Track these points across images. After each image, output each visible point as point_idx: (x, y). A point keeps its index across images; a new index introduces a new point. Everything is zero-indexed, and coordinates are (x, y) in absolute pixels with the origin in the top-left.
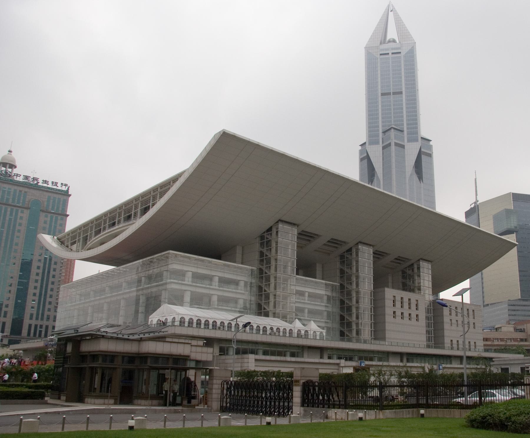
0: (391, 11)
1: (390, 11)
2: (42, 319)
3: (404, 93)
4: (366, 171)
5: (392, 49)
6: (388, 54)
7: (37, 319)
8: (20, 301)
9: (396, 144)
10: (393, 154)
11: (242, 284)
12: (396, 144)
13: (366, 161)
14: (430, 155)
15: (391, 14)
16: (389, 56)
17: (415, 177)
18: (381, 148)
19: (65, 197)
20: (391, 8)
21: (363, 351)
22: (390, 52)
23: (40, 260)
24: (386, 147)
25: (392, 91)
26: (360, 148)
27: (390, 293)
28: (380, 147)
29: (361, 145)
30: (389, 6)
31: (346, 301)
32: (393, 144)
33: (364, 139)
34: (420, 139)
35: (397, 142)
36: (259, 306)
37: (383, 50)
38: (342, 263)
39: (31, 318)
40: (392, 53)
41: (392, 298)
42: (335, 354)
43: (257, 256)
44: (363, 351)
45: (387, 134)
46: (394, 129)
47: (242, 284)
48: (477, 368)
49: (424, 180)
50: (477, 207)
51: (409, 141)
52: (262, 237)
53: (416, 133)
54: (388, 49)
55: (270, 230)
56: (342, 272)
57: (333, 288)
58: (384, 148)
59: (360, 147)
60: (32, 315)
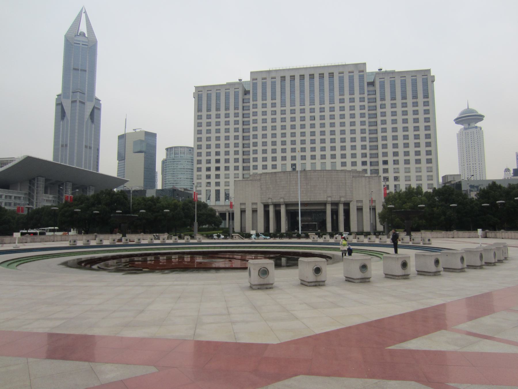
0: (84, 13)
1: (83, 12)
3: (87, 71)
5: (83, 41)
6: (79, 44)
10: (78, 108)
11: (22, 198)
13: (60, 107)
15: (83, 15)
16: (79, 46)
17: (90, 121)
20: (83, 11)
21: (418, 172)
22: (81, 43)
24: (73, 102)
26: (57, 97)
28: (70, 101)
29: (58, 95)
30: (82, 9)
31: (31, 199)
32: (78, 101)
33: (59, 91)
34: (94, 100)
35: (81, 100)
37: (77, 40)
40: (82, 44)
42: (197, 197)
43: (28, 187)
44: (418, 172)
46: (79, 92)
47: (22, 198)
49: (94, 123)
50: (125, 135)
54: (79, 41)
56: (30, 187)
59: (57, 96)
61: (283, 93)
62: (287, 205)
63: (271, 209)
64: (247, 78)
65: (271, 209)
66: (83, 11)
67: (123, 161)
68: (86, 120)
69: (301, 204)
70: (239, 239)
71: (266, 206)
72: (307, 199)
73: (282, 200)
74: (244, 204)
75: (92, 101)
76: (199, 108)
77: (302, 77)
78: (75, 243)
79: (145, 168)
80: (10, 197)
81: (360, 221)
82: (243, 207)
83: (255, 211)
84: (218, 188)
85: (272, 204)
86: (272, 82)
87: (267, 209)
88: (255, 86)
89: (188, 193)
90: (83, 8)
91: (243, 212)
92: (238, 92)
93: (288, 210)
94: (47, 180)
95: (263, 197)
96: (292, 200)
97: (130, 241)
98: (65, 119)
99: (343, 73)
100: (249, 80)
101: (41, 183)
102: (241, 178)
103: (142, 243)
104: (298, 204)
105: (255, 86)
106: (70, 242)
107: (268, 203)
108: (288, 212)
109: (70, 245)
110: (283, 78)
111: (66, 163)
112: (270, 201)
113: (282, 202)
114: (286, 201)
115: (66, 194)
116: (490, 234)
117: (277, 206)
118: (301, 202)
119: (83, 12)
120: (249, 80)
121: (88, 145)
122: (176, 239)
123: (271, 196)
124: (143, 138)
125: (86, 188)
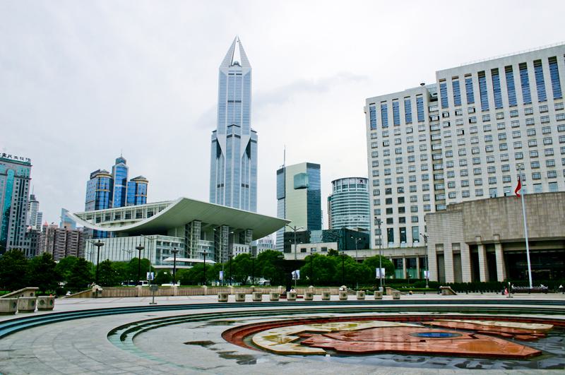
2: (17, 245)
4: (216, 149)
7: (14, 244)
8: (308, 278)
9: (236, 136)
10: (233, 142)
12: (236, 136)
13: (216, 143)
14: (256, 142)
15: (237, 44)
17: (246, 155)
18: (226, 137)
19: (29, 167)
20: (237, 40)
23: (15, 208)
25: (234, 103)
27: (235, 245)
32: (233, 135)
36: (186, 253)
38: (186, 228)
39: (11, 244)
41: (281, 366)
45: (230, 128)
48: (187, 263)
51: (243, 134)
52: (186, 225)
53: (248, 129)
55: (190, 223)
56: (186, 232)
57: (211, 243)
58: (228, 137)
60: (11, 242)
61: (483, 93)
62: (504, 244)
63: (481, 251)
64: (432, 81)
65: (481, 251)
66: (237, 40)
67: (283, 200)
68: (242, 155)
69: (529, 242)
70: (450, 294)
71: (473, 248)
72: (535, 236)
73: (496, 238)
74: (442, 245)
75: (248, 134)
76: (373, 126)
77: (495, 72)
78: (345, 297)
79: (309, 203)
80: (168, 243)
81: (457, 270)
82: (440, 249)
83: (457, 255)
84: (390, 226)
85: (483, 244)
86: (454, 83)
87: (475, 251)
88: (443, 88)
89: (364, 234)
90: (235, 41)
91: (440, 256)
92: (422, 98)
93: (415, 259)
94: (203, 224)
95: (467, 234)
96: (512, 236)
97: (298, 297)
98: (221, 156)
99: (470, 75)
100: (435, 82)
101: (198, 228)
102: (433, 210)
103: (383, 299)
104: (525, 242)
105: (443, 88)
106: (219, 297)
107: (493, 241)
108: (506, 256)
109: (219, 301)
110: (482, 75)
111: (222, 204)
112: (478, 240)
113: (496, 241)
114: (503, 238)
115: (536, 220)
116: (188, 289)
117: (489, 246)
118: (529, 239)
119: (237, 40)
120: (435, 82)
121: (245, 184)
122: (362, 295)
123: (479, 233)
124: (304, 170)
125: (244, 232)
